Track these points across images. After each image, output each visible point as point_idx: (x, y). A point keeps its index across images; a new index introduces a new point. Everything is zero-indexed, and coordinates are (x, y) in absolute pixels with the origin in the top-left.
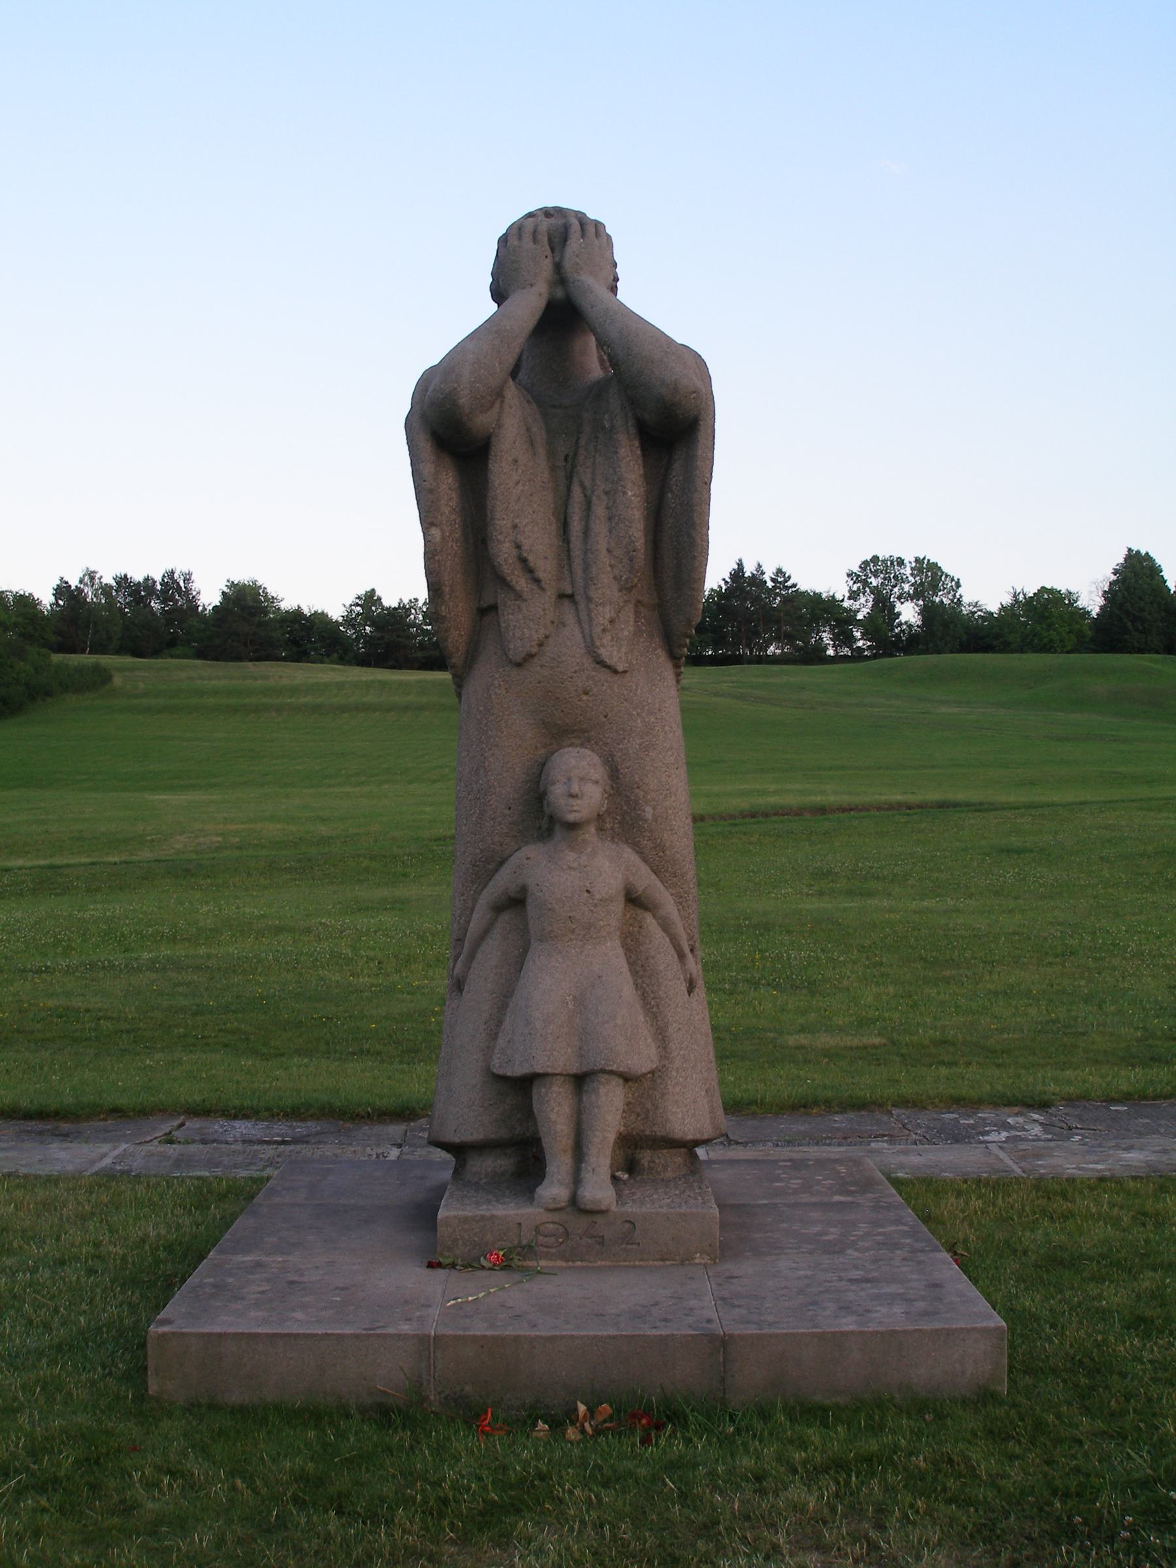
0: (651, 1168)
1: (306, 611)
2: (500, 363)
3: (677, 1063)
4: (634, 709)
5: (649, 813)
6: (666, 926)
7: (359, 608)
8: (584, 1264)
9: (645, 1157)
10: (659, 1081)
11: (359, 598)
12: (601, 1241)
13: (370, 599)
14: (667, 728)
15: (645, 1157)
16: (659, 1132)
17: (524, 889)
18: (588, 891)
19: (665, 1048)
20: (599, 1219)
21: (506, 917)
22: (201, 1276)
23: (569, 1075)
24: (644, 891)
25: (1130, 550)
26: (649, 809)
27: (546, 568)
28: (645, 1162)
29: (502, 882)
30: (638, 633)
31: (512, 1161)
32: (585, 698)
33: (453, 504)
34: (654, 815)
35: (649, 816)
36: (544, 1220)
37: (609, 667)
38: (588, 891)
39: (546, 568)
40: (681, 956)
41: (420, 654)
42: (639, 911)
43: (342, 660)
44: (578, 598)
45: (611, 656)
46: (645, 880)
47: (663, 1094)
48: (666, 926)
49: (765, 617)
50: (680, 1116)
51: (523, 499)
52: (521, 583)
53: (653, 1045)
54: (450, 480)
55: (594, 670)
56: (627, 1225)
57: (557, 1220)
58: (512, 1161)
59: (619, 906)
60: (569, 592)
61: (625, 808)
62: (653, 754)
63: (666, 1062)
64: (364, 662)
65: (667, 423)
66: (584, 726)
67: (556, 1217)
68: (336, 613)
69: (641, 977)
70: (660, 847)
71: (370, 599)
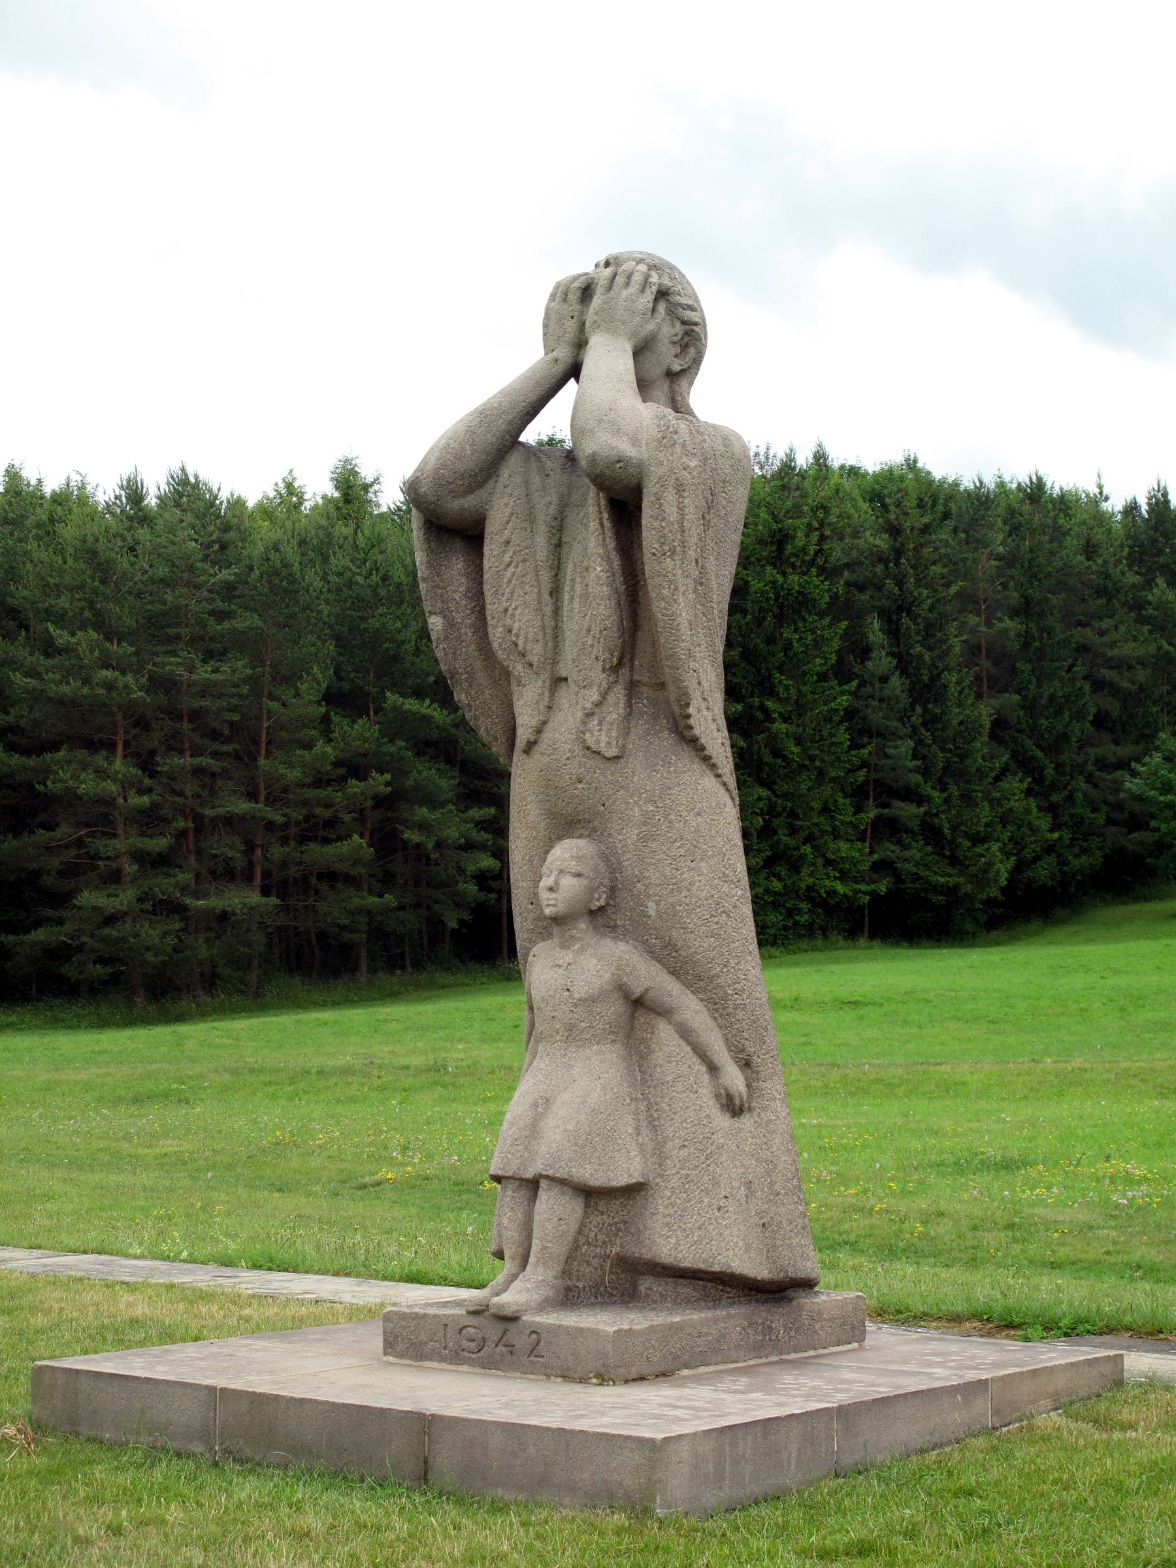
0: (647, 1296)
3: (674, 1183)
6: (685, 1033)
10: (651, 1200)
14: (672, 817)
15: (646, 1284)
16: (647, 1256)
20: (512, 1327)
23: (521, 1179)
26: (652, 905)
27: (536, 652)
28: (642, 1289)
32: (580, 786)
34: (657, 911)
35: (652, 912)
36: (466, 1323)
39: (536, 652)
40: (713, 1069)
42: (652, 1016)
45: (598, 742)
48: (685, 1033)
52: (518, 668)
55: (584, 756)
56: (534, 1336)
57: (476, 1324)
59: (615, 1009)
60: (564, 676)
66: (586, 816)
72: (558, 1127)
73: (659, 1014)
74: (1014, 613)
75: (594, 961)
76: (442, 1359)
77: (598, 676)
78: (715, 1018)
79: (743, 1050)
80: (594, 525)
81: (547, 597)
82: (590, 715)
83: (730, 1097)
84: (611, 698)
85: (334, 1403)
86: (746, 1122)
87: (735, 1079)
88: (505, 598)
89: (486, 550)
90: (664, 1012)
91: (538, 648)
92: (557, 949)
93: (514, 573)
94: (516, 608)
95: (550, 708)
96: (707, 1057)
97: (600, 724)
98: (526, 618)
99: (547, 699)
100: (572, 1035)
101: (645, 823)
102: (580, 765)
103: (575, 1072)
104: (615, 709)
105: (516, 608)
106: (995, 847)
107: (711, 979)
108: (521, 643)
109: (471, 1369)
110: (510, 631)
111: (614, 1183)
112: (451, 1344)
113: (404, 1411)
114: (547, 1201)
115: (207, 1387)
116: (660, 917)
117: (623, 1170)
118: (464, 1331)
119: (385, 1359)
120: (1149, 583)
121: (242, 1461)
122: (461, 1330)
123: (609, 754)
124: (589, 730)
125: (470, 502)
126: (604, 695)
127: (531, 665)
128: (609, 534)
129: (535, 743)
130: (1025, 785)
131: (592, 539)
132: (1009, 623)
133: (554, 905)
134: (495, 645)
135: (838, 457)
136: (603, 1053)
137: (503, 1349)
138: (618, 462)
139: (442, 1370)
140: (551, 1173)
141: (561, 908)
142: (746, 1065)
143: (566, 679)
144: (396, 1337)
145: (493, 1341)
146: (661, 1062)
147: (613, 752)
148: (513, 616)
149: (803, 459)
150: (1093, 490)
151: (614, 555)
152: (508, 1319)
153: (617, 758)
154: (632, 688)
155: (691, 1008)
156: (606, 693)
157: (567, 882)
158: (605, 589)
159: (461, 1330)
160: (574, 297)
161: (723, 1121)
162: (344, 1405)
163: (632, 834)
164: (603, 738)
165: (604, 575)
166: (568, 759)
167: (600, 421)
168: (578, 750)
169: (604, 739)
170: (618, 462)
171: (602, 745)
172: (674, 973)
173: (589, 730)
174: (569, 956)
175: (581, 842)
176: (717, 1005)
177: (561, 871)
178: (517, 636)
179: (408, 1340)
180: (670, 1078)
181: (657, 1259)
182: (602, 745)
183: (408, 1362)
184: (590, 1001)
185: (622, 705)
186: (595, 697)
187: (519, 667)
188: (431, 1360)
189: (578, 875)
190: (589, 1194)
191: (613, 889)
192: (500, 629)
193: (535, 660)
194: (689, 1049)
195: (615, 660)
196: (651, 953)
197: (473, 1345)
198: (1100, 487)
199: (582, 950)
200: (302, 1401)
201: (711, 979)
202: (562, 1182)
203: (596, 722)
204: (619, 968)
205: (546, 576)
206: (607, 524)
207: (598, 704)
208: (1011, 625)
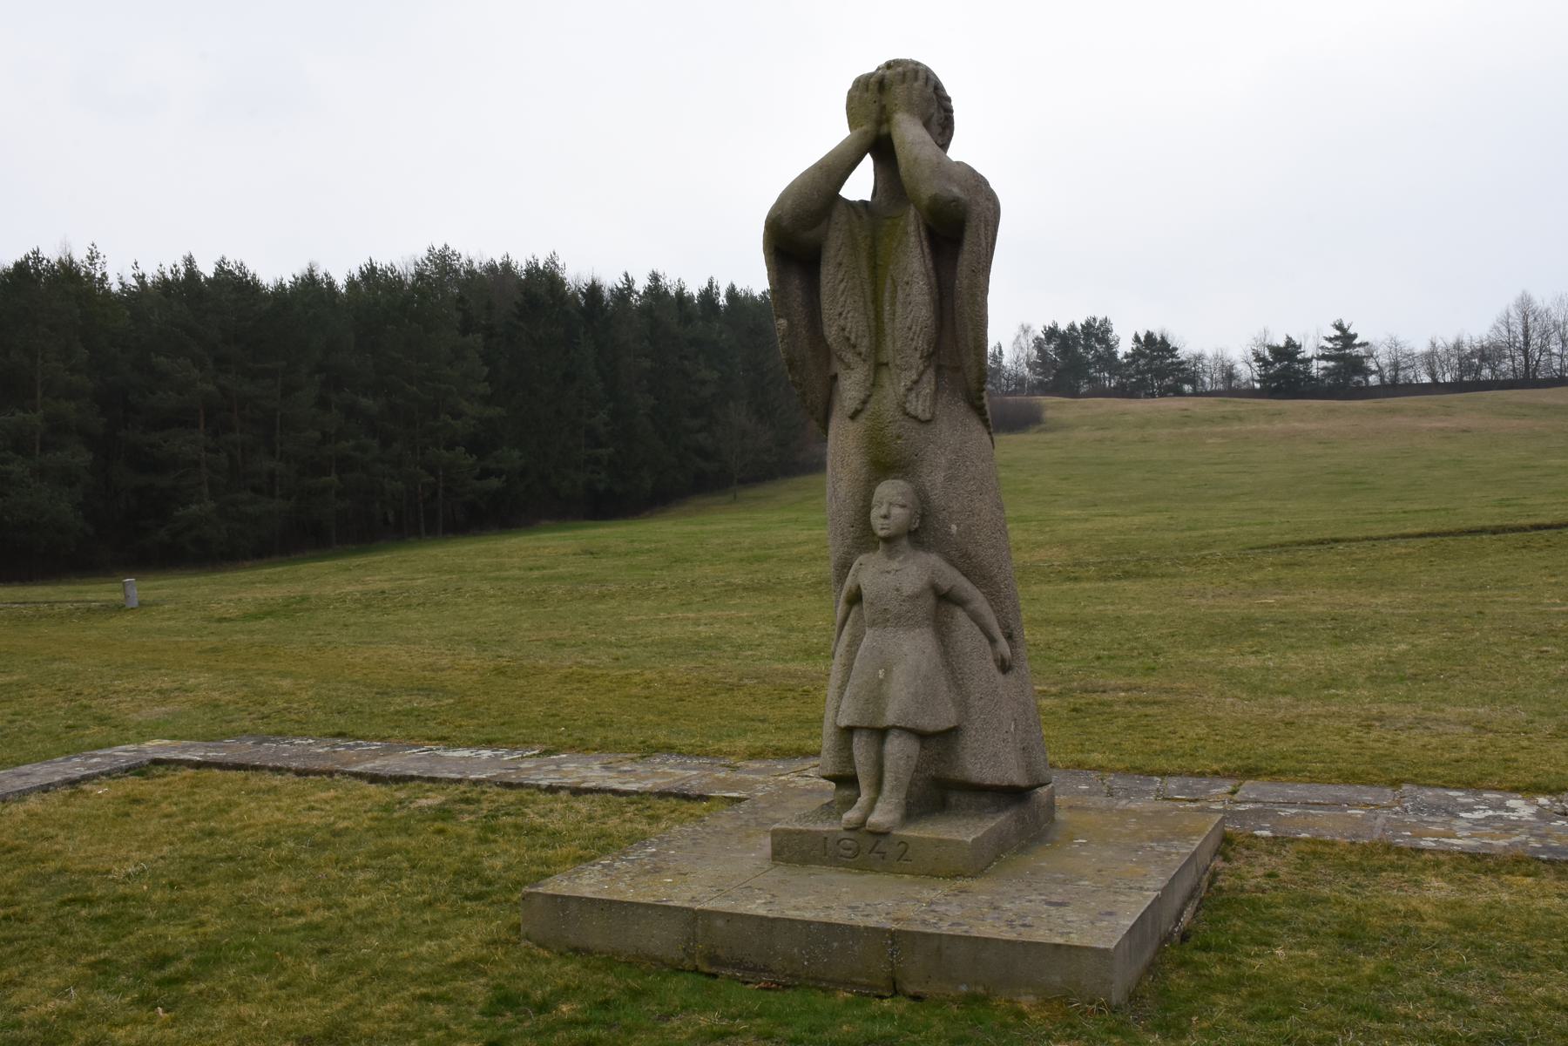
6: (975, 618)
9: (953, 798)
12: (883, 855)
15: (953, 798)
16: (956, 774)
21: (855, 608)
27: (864, 345)
30: (937, 391)
37: (915, 418)
40: (993, 641)
46: (953, 578)
48: (975, 618)
52: (849, 356)
59: (931, 601)
67: (852, 835)
77: (916, 360)
82: (910, 390)
83: (1003, 660)
84: (925, 378)
86: (1011, 678)
87: (1004, 646)
90: (961, 603)
91: (865, 342)
100: (901, 621)
104: (927, 389)
108: (853, 338)
117: (944, 718)
126: (921, 375)
128: (928, 257)
131: (913, 263)
134: (830, 340)
135: (670, 281)
141: (892, 531)
142: (1009, 637)
145: (867, 851)
147: (928, 416)
149: (641, 285)
151: (932, 273)
152: (880, 834)
153: (928, 422)
154: (939, 370)
155: (979, 601)
157: (896, 511)
161: (1000, 677)
163: (939, 477)
164: (919, 406)
168: (899, 416)
169: (920, 408)
174: (895, 565)
175: (901, 482)
176: (994, 597)
179: (793, 851)
184: (915, 597)
189: (903, 506)
190: (922, 736)
191: (923, 517)
196: (951, 562)
199: (905, 560)
202: (900, 728)
205: (868, 288)
206: (927, 250)
207: (916, 382)
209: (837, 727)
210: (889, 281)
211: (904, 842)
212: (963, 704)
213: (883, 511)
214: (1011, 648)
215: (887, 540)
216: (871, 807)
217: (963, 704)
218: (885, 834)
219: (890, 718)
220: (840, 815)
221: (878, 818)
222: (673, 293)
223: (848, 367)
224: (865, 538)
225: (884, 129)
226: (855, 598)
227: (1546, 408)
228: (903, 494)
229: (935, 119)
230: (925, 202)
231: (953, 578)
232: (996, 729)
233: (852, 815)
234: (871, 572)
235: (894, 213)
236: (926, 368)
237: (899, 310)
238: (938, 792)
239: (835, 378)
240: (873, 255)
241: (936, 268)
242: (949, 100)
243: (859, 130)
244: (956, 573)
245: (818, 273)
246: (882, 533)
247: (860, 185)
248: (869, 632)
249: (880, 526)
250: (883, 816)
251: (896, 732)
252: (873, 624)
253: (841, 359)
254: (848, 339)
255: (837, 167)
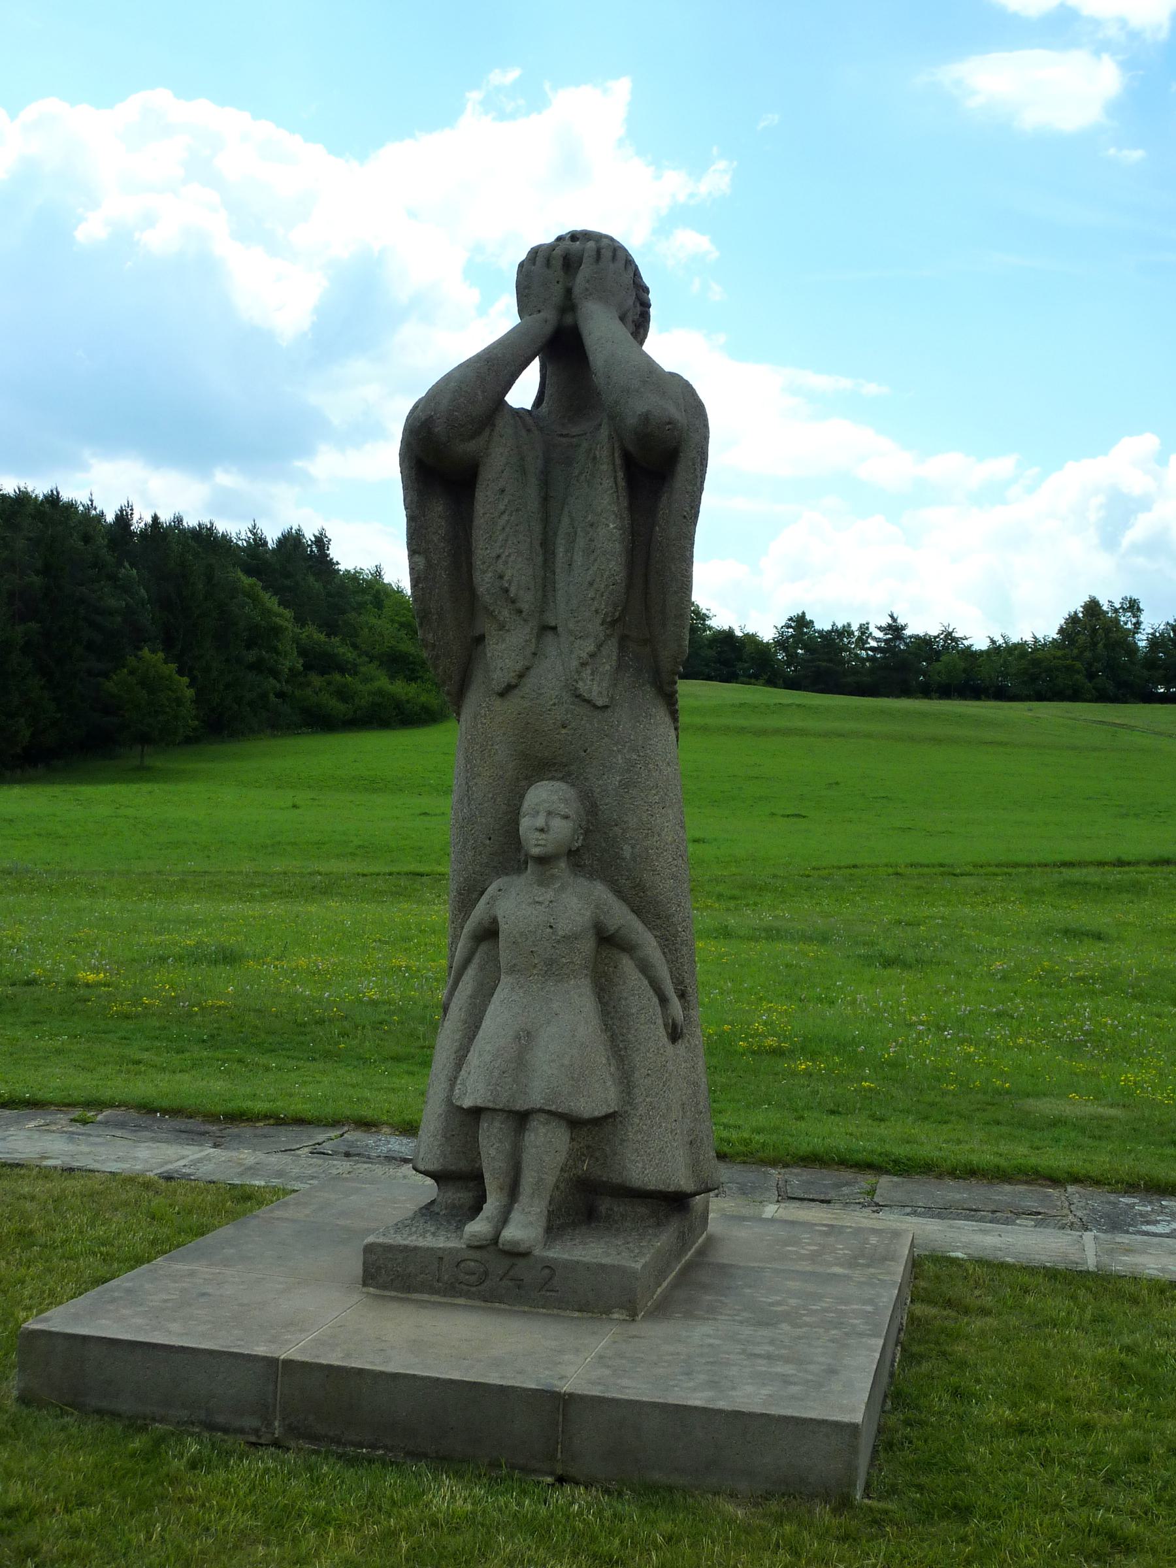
1: (738, 633)
2: (483, 392)
3: (642, 1110)
4: (616, 744)
5: (627, 852)
6: (645, 968)
7: (791, 630)
8: (503, 1306)
9: (605, 1205)
11: (791, 619)
12: (519, 1284)
13: (801, 622)
15: (605, 1205)
16: (616, 1179)
17: (495, 921)
18: (551, 927)
19: (629, 1093)
20: (521, 1263)
21: (484, 947)
22: (125, 1281)
23: (510, 1112)
24: (617, 931)
25: (804, 613)
27: (527, 601)
28: (603, 1209)
29: (479, 911)
30: (620, 667)
31: (471, 1194)
32: (564, 731)
33: (442, 532)
37: (588, 701)
38: (551, 927)
39: (527, 601)
40: (663, 1001)
41: (849, 679)
43: (771, 683)
44: (560, 629)
45: (590, 691)
46: (620, 916)
47: (623, 1141)
48: (645, 968)
49: (732, 657)
50: (640, 1165)
51: (507, 529)
52: (505, 614)
53: (613, 1089)
54: (440, 509)
55: (573, 703)
56: (547, 1271)
58: (471, 1194)
59: (587, 945)
60: (553, 624)
61: (604, 845)
62: (634, 792)
63: (628, 1108)
64: (792, 684)
65: (660, 456)
66: (564, 760)
67: (477, 1255)
68: (767, 635)
69: (612, 1018)
70: (639, 887)
71: (801, 622)
72: (553, 1061)
73: (624, 950)
74: (37, 573)
75: (575, 900)
76: (433, 1291)
77: (595, 627)
78: (664, 953)
79: (682, 982)
80: (608, 483)
81: (538, 548)
82: (583, 665)
83: (675, 1026)
84: (605, 651)
85: (438, 1379)
86: (681, 1047)
88: (498, 544)
89: (480, 495)
92: (535, 886)
93: (508, 521)
94: (509, 556)
95: (535, 654)
96: (660, 988)
97: (592, 674)
98: (519, 566)
99: (533, 646)
100: (552, 969)
101: (628, 771)
102: (567, 711)
103: (555, 1006)
105: (509, 556)
106: (22, 720)
107: (668, 917)
109: (470, 1302)
110: (501, 577)
111: (596, 1114)
112: (446, 1277)
113: (530, 1389)
114: (545, 1135)
115: (265, 1358)
116: (635, 861)
118: (462, 1265)
119: (365, 1290)
120: (120, 564)
121: (313, 1438)
122: (458, 1265)
123: (600, 703)
124: (582, 679)
125: (471, 446)
126: (599, 646)
127: (521, 612)
129: (516, 686)
130: (42, 683)
132: (35, 579)
133: (545, 846)
134: (481, 590)
136: (579, 987)
137: (510, 1284)
138: (669, 423)
139: (434, 1303)
140: (553, 1108)
141: (550, 849)
142: (682, 995)
143: (554, 628)
144: (379, 1268)
145: (501, 1281)
146: (625, 995)
148: (506, 562)
150: (87, 502)
151: (625, 514)
152: (516, 1254)
154: (623, 640)
156: (601, 645)
157: (557, 823)
158: (617, 545)
159: (458, 1265)
160: (557, 264)
161: (670, 1048)
162: (452, 1381)
164: (594, 688)
165: (617, 533)
166: (554, 704)
167: (644, 382)
170: (669, 423)
171: (594, 694)
172: (636, 911)
173: (582, 679)
174: (550, 895)
177: (549, 813)
178: (510, 582)
179: (390, 1273)
180: (634, 1011)
181: (628, 1184)
182: (594, 694)
183: (393, 1294)
185: (615, 658)
186: (592, 648)
187: (506, 613)
188: (421, 1292)
189: (566, 817)
190: (574, 1123)
192: (490, 575)
193: (525, 607)
194: (646, 982)
195: (617, 614)
196: (619, 893)
197: (473, 1279)
198: (92, 501)
199: (563, 888)
200: (395, 1376)
201: (668, 917)
202: (549, 1112)
203: (589, 671)
204: (597, 907)
205: (537, 528)
206: (622, 483)
207: (592, 655)
208: (37, 580)
209: (449, 1101)
210: (565, 520)
211: (550, 1266)
212: (626, 1082)
213: (540, 822)
214: (684, 1009)
215: (543, 861)
216: (504, 1219)
217: (626, 1082)
218: (525, 1255)
219: (536, 1098)
220: (460, 1228)
221: (513, 1233)
222: (110, 518)
223: (502, 627)
224: (504, 852)
225: (568, 320)
226: (489, 933)
227: (882, 712)
228: (566, 801)
229: (630, 314)
230: (632, 421)
231: (620, 916)
232: (663, 1116)
233: (478, 1227)
234: (514, 903)
235: (569, 429)
236: (608, 637)
237: (578, 559)
238: (590, 1200)
239: (480, 639)
240: (546, 483)
241: (632, 508)
242: (647, 290)
243: (527, 318)
244: (625, 909)
245: (472, 497)
246: (535, 851)
247: (524, 392)
248: (505, 979)
249: (534, 843)
250: (523, 1229)
251: (542, 1117)
252: (512, 970)
253: (491, 614)
254: (507, 591)
255: (498, 366)
